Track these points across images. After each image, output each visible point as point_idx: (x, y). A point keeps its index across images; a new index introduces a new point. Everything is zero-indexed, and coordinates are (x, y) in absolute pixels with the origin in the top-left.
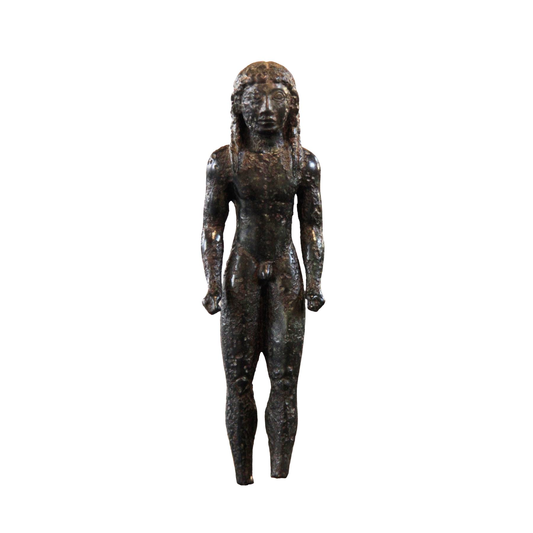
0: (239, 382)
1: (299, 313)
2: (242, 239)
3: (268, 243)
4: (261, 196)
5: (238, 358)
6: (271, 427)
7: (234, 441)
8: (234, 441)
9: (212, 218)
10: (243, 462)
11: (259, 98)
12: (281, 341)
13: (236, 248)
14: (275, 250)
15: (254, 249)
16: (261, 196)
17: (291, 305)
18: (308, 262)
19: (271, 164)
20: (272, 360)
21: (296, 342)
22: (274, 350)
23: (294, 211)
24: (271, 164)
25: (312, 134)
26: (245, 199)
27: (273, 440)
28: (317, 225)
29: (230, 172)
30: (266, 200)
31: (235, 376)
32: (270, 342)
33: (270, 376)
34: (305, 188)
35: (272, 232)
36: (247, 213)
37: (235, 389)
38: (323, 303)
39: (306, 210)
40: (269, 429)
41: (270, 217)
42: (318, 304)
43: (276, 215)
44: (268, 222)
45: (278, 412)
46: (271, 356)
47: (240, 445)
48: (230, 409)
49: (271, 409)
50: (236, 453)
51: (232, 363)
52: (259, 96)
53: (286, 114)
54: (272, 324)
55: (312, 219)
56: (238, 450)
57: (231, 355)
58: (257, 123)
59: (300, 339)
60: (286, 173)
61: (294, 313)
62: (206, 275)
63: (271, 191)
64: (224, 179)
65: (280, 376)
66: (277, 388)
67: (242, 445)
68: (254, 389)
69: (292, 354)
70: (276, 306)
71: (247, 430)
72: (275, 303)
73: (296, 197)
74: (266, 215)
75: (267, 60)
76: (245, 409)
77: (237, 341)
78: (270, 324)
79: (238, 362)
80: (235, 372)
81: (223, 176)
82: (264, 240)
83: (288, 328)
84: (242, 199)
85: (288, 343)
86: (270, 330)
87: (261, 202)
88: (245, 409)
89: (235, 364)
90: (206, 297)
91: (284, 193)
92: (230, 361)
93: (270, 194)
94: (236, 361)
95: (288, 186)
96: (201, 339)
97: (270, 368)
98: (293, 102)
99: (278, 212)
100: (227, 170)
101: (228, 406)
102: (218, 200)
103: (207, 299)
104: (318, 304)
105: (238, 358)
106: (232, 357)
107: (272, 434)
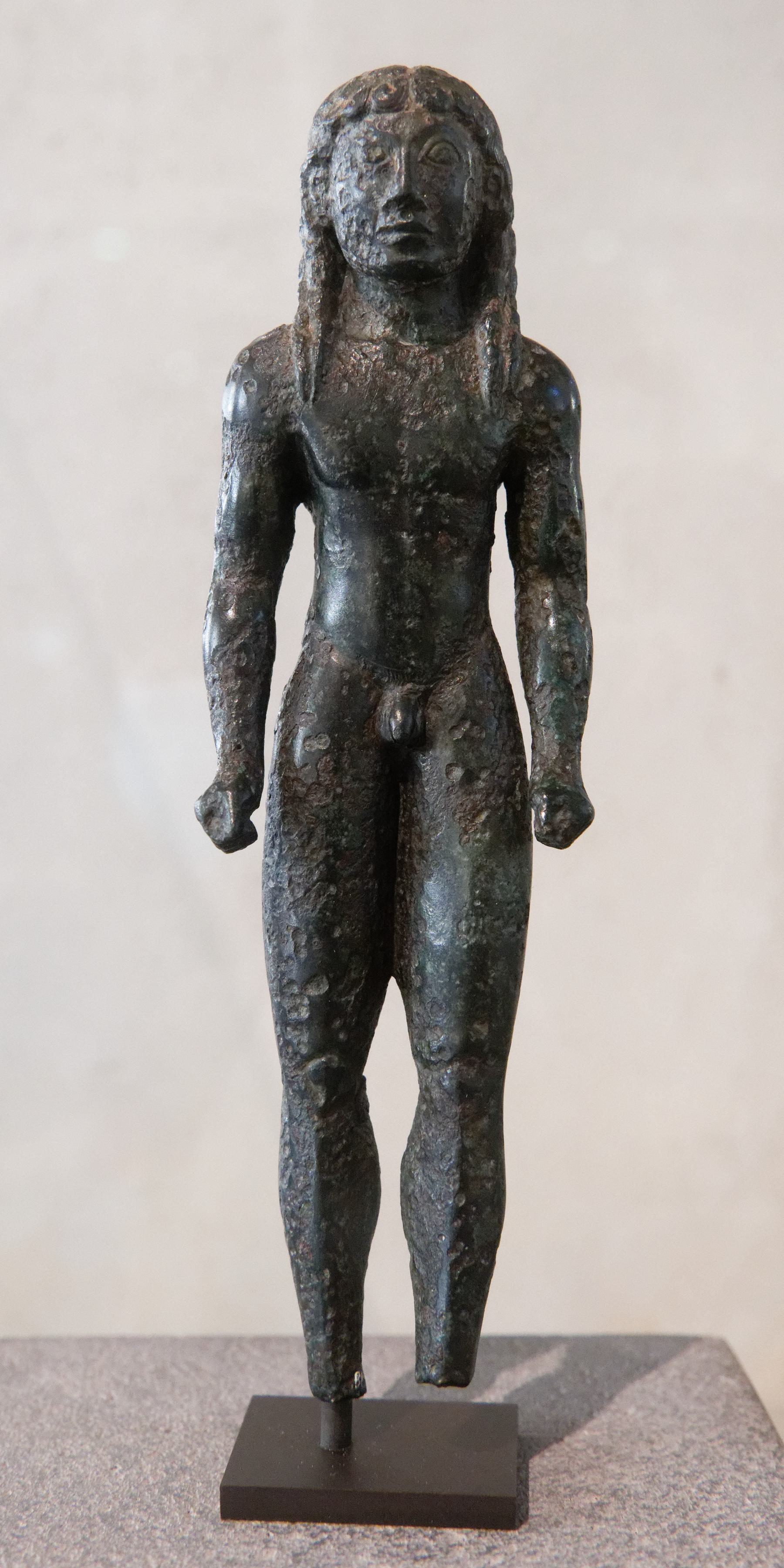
0: (316, 1071)
1: (509, 846)
2: (333, 612)
3: (410, 624)
4: (388, 474)
5: (313, 992)
6: (420, 1220)
7: (303, 1257)
8: (303, 1257)
9: (237, 548)
10: (329, 1329)
11: (380, 159)
12: (452, 942)
13: (312, 644)
14: (433, 647)
15: (365, 644)
16: (388, 474)
17: (484, 824)
18: (539, 691)
19: (424, 376)
20: (422, 1002)
21: (498, 944)
22: (429, 968)
23: (496, 532)
24: (424, 376)
25: (552, 294)
26: (337, 485)
27: (425, 1261)
28: (569, 576)
29: (288, 400)
30: (403, 489)
31: (304, 1050)
32: (415, 942)
33: (417, 1054)
34: (529, 442)
35: (424, 590)
36: (346, 531)
37: (303, 1094)
38: (500, 1512)
39: (534, 526)
40: (414, 1224)
41: (417, 544)
42: (572, 817)
43: (435, 536)
44: (411, 558)
45: (440, 1172)
46: (420, 990)
47: (319, 1273)
48: (291, 1155)
49: (419, 1159)
50: (306, 1295)
51: (296, 1008)
52: (378, 152)
53: (466, 217)
54: (422, 885)
55: (556, 560)
56: (314, 1287)
57: (291, 982)
58: (372, 240)
59: (513, 935)
60: (468, 405)
61: (491, 850)
62: (214, 728)
63: (419, 458)
64: (274, 424)
65: (447, 1055)
66: (436, 1094)
67: (327, 1273)
68: (371, 1092)
69: (486, 983)
70: (435, 830)
71: (342, 1224)
72: (432, 819)
73: (502, 493)
74: (404, 535)
75: (412, 63)
76: (338, 1156)
77: (310, 939)
78: (416, 885)
79: (313, 1005)
80: (305, 1038)
81: (268, 413)
82: (399, 616)
83: (474, 898)
84: (328, 484)
85: (470, 947)
86: (419, 904)
87: (386, 495)
88: (338, 1156)
89: (305, 1014)
90: (207, 793)
91: (461, 465)
92: (287, 1004)
93: (416, 468)
94: (306, 1001)
95: (474, 444)
96: (222, 923)
97: (417, 1028)
98: (492, 188)
99: (442, 527)
100: (283, 393)
101: (285, 1144)
102: (256, 490)
103: (209, 800)
104: (572, 817)
105: (313, 992)
106: (295, 989)
107: (420, 1243)
